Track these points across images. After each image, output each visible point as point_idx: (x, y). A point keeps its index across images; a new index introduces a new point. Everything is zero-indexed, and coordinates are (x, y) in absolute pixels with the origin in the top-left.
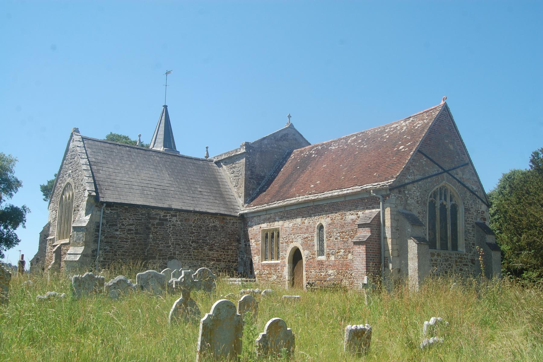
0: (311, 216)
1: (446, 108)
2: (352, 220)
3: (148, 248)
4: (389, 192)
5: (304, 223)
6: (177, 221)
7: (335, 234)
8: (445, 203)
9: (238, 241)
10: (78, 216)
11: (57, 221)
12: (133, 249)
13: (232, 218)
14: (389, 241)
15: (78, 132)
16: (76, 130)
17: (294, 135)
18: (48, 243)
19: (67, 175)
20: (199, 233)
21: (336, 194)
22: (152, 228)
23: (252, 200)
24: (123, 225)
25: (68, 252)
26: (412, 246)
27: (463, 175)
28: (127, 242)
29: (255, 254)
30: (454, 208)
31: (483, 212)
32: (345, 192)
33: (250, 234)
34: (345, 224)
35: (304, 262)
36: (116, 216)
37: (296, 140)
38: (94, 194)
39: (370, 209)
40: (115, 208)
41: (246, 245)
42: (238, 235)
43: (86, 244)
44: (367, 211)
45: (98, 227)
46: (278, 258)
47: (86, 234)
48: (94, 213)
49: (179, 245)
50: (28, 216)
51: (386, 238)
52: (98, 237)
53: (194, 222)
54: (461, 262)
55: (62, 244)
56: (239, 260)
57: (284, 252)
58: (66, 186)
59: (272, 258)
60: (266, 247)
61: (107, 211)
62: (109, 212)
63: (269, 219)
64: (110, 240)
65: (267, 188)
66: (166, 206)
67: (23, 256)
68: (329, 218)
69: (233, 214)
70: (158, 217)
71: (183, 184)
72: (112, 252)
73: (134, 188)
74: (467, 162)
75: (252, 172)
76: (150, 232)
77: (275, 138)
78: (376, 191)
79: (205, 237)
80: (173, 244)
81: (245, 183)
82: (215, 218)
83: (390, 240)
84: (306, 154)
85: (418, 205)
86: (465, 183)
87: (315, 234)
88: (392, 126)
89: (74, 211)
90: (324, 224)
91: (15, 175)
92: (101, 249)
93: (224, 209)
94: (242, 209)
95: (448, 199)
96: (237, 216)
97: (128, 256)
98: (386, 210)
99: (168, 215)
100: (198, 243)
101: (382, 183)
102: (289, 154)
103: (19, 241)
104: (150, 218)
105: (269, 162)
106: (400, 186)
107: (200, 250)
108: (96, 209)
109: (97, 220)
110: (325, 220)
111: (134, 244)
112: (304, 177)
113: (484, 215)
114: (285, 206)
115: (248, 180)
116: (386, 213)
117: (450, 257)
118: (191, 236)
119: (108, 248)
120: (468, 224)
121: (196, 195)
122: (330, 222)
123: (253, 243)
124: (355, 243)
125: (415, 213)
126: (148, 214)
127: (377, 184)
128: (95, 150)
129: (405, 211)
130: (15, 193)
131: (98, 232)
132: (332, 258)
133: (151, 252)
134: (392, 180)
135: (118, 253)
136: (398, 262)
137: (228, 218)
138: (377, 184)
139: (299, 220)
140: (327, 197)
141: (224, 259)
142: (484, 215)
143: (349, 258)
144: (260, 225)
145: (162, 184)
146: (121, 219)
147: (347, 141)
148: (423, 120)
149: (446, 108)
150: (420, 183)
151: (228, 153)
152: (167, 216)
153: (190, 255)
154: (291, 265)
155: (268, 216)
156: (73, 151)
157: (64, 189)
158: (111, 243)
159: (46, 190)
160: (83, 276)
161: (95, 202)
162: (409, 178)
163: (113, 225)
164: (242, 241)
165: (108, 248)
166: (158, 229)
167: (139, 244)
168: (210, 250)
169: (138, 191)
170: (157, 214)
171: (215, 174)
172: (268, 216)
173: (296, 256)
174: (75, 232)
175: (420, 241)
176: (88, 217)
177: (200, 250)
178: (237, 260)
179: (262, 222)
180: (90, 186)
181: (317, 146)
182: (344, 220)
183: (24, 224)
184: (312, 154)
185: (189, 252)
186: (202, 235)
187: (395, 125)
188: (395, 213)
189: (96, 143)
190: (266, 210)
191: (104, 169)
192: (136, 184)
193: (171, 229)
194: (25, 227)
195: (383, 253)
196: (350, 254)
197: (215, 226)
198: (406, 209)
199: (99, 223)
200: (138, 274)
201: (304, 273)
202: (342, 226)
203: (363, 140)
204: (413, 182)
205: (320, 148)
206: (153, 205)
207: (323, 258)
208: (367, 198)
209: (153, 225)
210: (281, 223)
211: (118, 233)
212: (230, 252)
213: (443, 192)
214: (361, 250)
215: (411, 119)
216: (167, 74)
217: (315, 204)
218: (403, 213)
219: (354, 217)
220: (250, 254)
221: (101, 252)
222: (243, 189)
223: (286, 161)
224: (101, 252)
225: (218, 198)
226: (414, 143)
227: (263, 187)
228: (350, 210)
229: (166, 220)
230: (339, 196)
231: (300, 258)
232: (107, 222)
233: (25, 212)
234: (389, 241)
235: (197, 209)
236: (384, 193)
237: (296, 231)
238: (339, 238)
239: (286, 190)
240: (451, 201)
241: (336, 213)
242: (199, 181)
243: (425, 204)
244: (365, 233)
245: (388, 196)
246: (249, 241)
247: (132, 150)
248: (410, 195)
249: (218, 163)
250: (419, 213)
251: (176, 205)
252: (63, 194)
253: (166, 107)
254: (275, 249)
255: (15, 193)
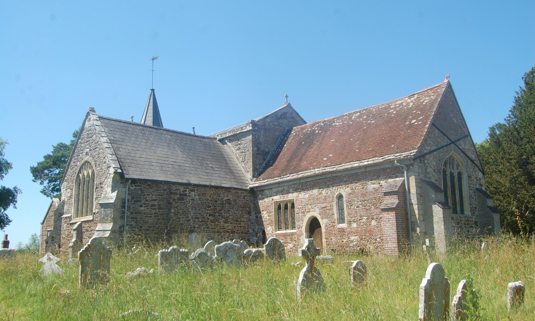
0: (328, 187)
1: (449, 86)
2: (374, 189)
3: (170, 223)
4: (412, 162)
5: (321, 193)
6: (195, 195)
7: (357, 202)
8: (453, 172)
9: (249, 213)
10: (104, 193)
11: (73, 199)
12: (157, 224)
13: (243, 191)
14: (416, 207)
15: (94, 112)
16: (92, 110)
17: (292, 113)
18: (63, 221)
19: (84, 153)
20: (215, 206)
21: (356, 165)
22: (174, 203)
23: (260, 174)
24: (147, 200)
25: (97, 229)
26: (438, 211)
27: (465, 145)
28: (151, 217)
29: (268, 225)
30: (460, 174)
31: (480, 179)
32: (366, 163)
33: (261, 206)
34: (367, 192)
35: (323, 230)
36: (140, 192)
37: (293, 118)
38: (120, 171)
39: (393, 178)
40: (138, 184)
41: (257, 217)
42: (249, 208)
43: (114, 220)
44: (390, 180)
45: (124, 203)
46: (293, 228)
47: (114, 210)
48: (120, 190)
49: (198, 218)
50: (19, 198)
51: (412, 204)
52: (124, 213)
53: (210, 197)
54: (468, 224)
55: (82, 222)
56: (251, 231)
57: (301, 222)
58: (84, 164)
59: (287, 228)
60: (279, 218)
61: (131, 188)
62: (133, 188)
63: (282, 191)
64: (135, 215)
65: (274, 162)
66: (185, 181)
67: (7, 236)
68: (349, 188)
69: (244, 188)
70: (178, 193)
71: (196, 161)
72: (138, 228)
73: (156, 165)
74: (466, 134)
75: (258, 148)
76: (171, 207)
77: (276, 116)
78: (399, 161)
79: (220, 210)
80: (192, 218)
81: (253, 159)
82: (229, 192)
83: (417, 206)
84: (308, 131)
85: (434, 173)
86: (467, 153)
87: (334, 204)
88: (397, 103)
89: (97, 188)
90: (344, 194)
91: (5, 158)
92: (127, 225)
93: (236, 184)
94: (252, 184)
95: (455, 167)
96: (247, 190)
97: (152, 230)
98: (410, 178)
99: (187, 190)
100: (214, 216)
101: (404, 154)
102: (290, 131)
103: (10, 221)
104: (172, 194)
105: (272, 139)
106: (421, 156)
107: (217, 223)
108: (121, 186)
109: (123, 197)
110: (344, 191)
111: (158, 219)
112: (312, 152)
113: (481, 181)
114: (300, 179)
115: (255, 156)
116: (410, 181)
117: (461, 220)
118: (208, 210)
119: (134, 223)
120: (471, 189)
121: (208, 171)
122: (350, 191)
123: (265, 215)
124: (383, 210)
125: (433, 180)
126: (169, 189)
127: (399, 154)
128: (112, 129)
129: (426, 179)
130: (6, 174)
131: (125, 208)
132: (354, 225)
133: (173, 226)
134: (415, 151)
135: (143, 228)
136: (423, 226)
137: (240, 192)
138: (399, 154)
139: (315, 191)
140: (347, 168)
141: (238, 231)
142: (481, 181)
143: (373, 224)
144: (272, 197)
145: (178, 161)
146: (145, 195)
147: (351, 118)
148: (430, 96)
149: (449, 86)
150: (435, 153)
151: (233, 131)
152: (186, 191)
153: (208, 228)
154: (308, 233)
155: (281, 189)
156: (90, 130)
157: (81, 168)
158: (137, 218)
159: (36, 171)
160: (169, 250)
161: (121, 179)
162: (427, 148)
163: (138, 201)
164: (253, 213)
165: (134, 223)
166: (179, 203)
167: (163, 219)
168: (225, 223)
169: (158, 168)
170: (177, 189)
171: (221, 150)
172: (281, 189)
173: (314, 226)
174: (102, 209)
175: (444, 205)
176: (115, 194)
177: (217, 223)
178: (249, 231)
179: (275, 194)
180: (114, 163)
181: (318, 123)
182: (366, 189)
183: (15, 205)
184: (315, 130)
185: (207, 225)
186: (218, 208)
187: (400, 102)
188: (418, 181)
189: (112, 122)
190: (279, 183)
191: (123, 147)
192: (154, 161)
193: (190, 203)
194: (15, 208)
195: (409, 218)
196: (373, 221)
197: (228, 200)
198: (426, 177)
199: (124, 199)
200: (216, 246)
201: (324, 240)
202: (364, 195)
203: (368, 116)
204: (430, 152)
205: (322, 124)
206: (174, 180)
207: (344, 225)
208: (389, 168)
209: (174, 200)
210: (295, 194)
211: (142, 208)
212: (243, 224)
213: (450, 161)
214: (391, 216)
215: (416, 96)
216: (153, 59)
217: (333, 176)
218: (425, 181)
219: (376, 186)
220: (263, 225)
221: (127, 228)
222: (250, 164)
223: (288, 138)
224: (127, 228)
225: (228, 173)
226: (427, 117)
227: (269, 162)
228: (372, 180)
229: (186, 195)
230: (360, 167)
231: (319, 226)
232: (132, 198)
233: (17, 193)
234: (416, 207)
235: (213, 184)
236: (408, 163)
237: (312, 201)
238: (361, 206)
239: (297, 164)
240: (457, 169)
241: (357, 183)
242: (208, 157)
243: (440, 172)
244: (393, 201)
245: (412, 165)
246: (260, 213)
247: (145, 128)
248: (429, 164)
249: (222, 141)
250: (436, 180)
251: (194, 181)
252: (80, 172)
253: (153, 90)
254: (290, 219)
255: (6, 174)
